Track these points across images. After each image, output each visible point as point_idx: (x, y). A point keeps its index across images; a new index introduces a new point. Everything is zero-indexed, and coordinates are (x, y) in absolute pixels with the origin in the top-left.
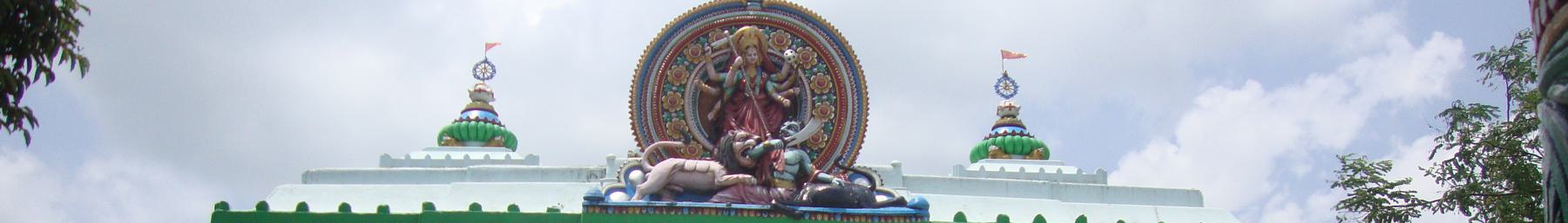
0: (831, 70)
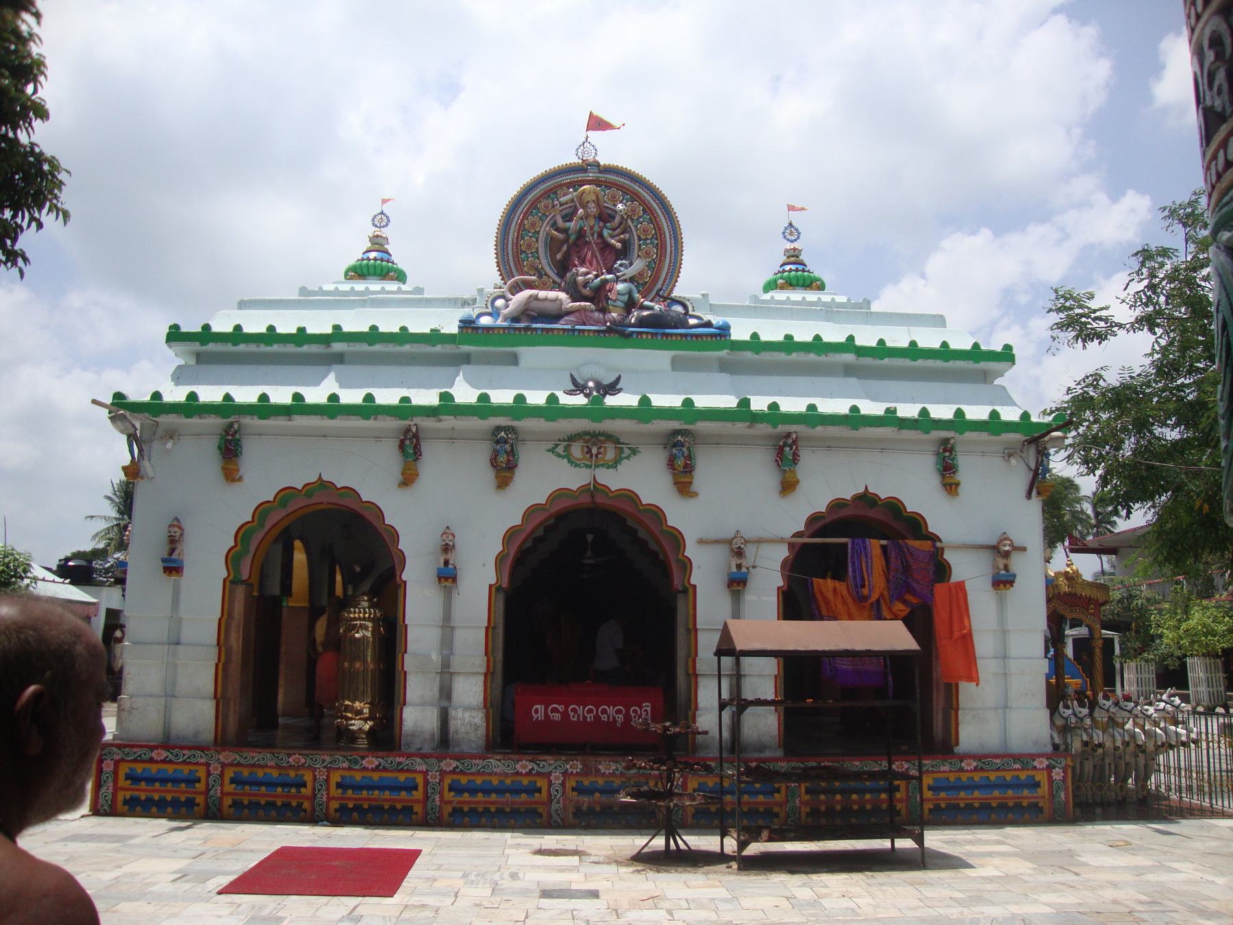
0: (654, 220)
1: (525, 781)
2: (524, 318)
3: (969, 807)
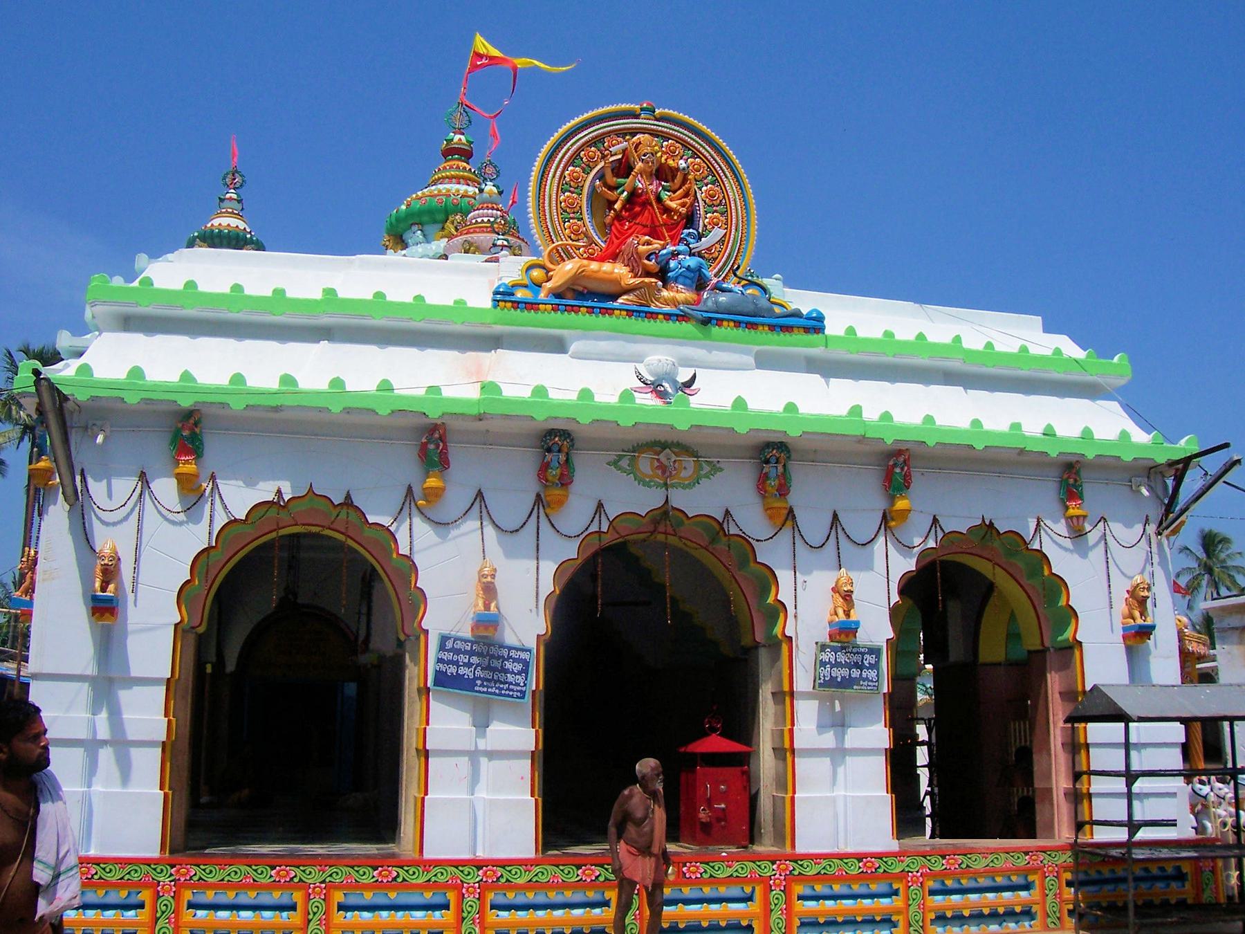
2: (569, 294)
3: (1165, 904)
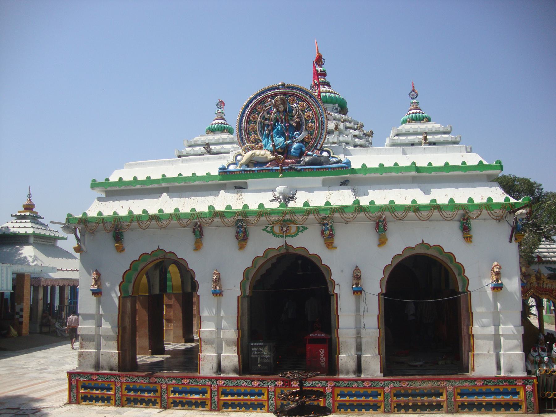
1: (257, 390)
2: (251, 164)
